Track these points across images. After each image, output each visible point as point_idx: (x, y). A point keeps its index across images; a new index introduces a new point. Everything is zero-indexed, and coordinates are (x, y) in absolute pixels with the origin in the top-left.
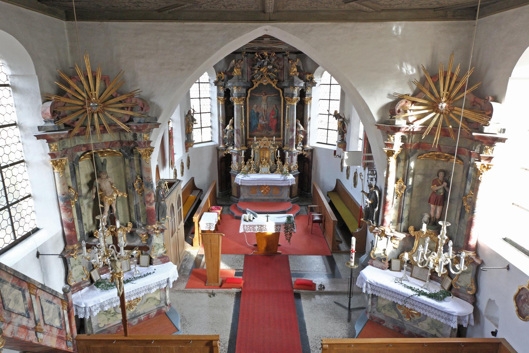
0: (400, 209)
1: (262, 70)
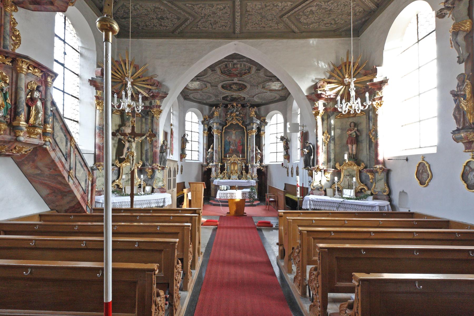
0: (328, 153)
1: (232, 115)
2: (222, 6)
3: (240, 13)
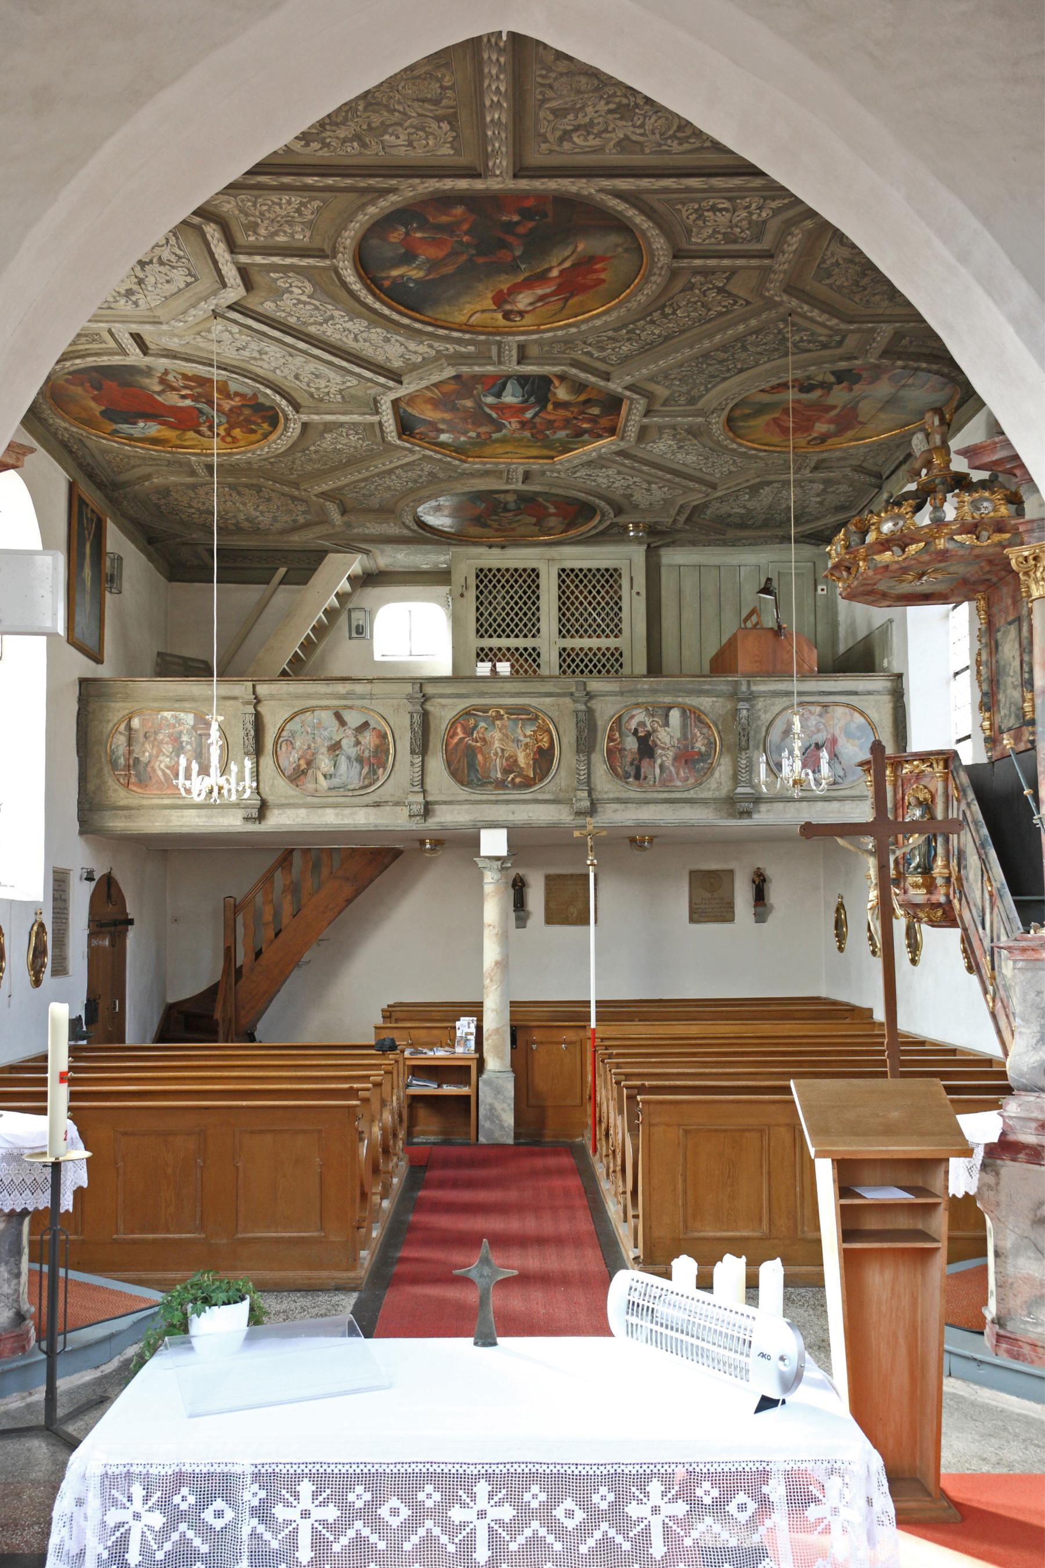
2: (574, 143)
3: (488, 119)
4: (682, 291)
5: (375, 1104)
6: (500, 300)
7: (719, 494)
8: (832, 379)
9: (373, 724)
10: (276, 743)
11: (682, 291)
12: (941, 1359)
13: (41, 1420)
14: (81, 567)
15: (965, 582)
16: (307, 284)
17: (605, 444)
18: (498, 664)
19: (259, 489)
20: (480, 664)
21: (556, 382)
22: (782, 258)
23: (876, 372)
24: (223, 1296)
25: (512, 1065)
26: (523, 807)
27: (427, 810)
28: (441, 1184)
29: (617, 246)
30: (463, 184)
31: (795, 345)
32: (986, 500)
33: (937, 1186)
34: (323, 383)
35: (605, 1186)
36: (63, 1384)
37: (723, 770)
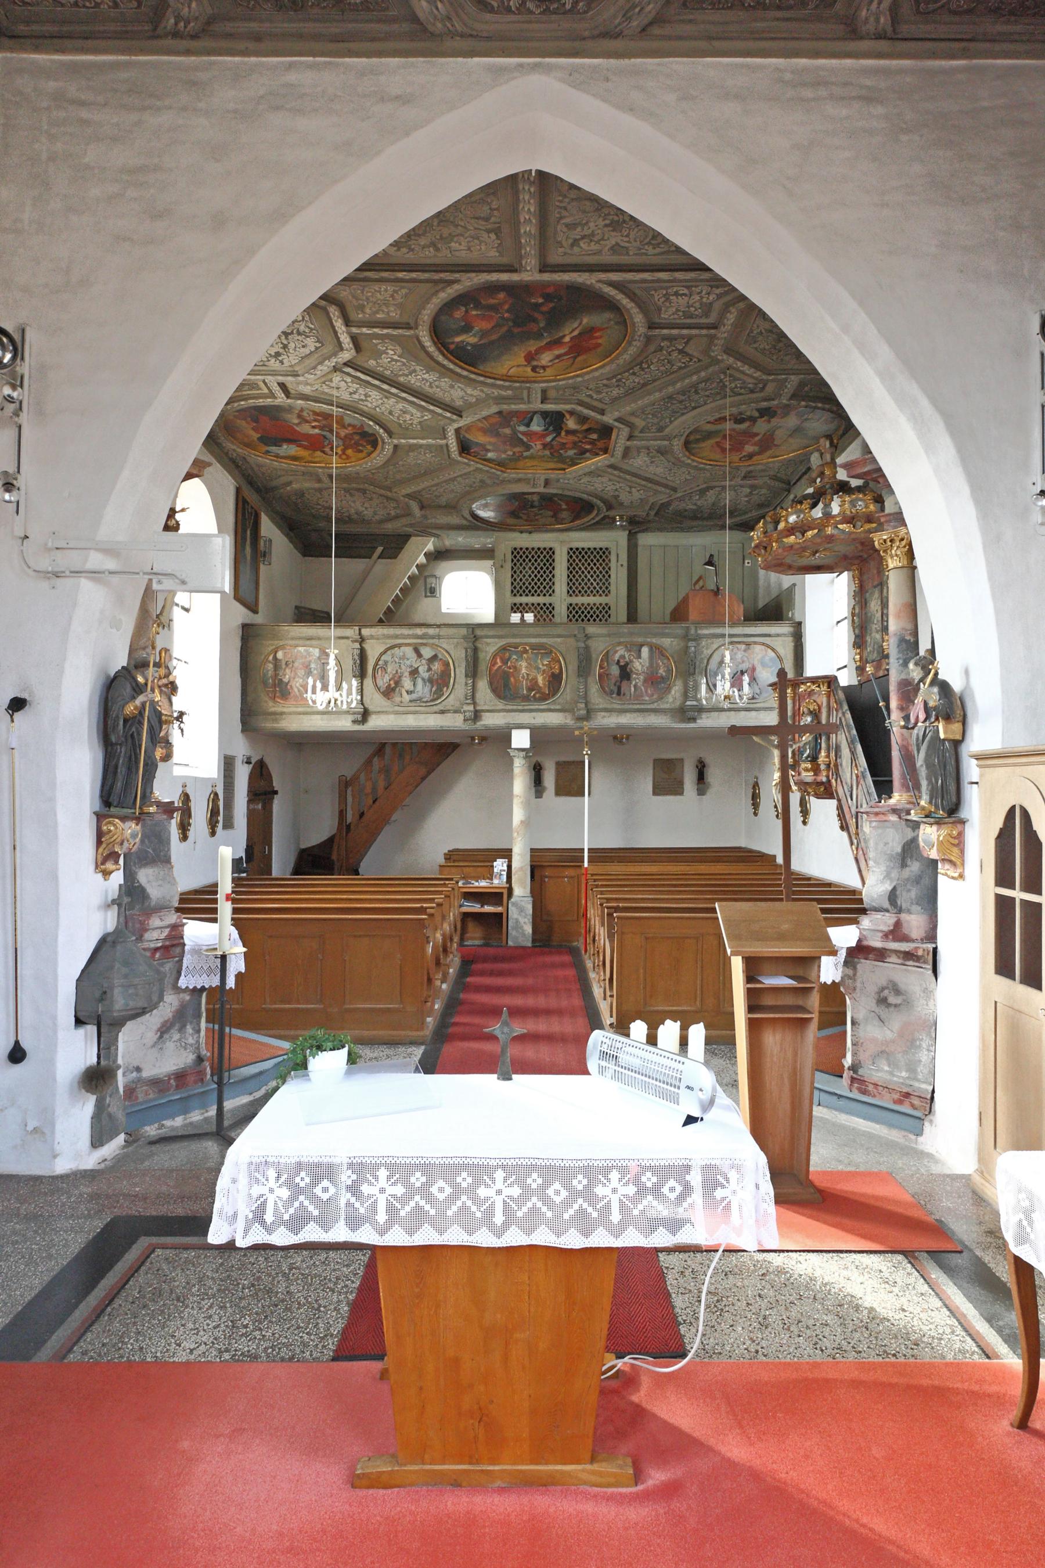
3: (522, 231)
4: (655, 352)
5: (438, 918)
6: (530, 358)
7: (679, 495)
8: (757, 414)
9: (440, 656)
10: (374, 669)
11: (655, 352)
12: (812, 1094)
13: (214, 1128)
14: (244, 548)
15: (845, 557)
16: (398, 347)
17: (600, 460)
18: (526, 615)
19: (364, 491)
20: (513, 615)
21: (568, 416)
22: (723, 329)
23: (787, 409)
24: (330, 1045)
25: (532, 892)
26: (540, 714)
27: (477, 715)
28: (482, 973)
29: (610, 320)
30: (504, 277)
31: (732, 390)
32: (861, 500)
33: (813, 976)
34: (408, 417)
35: (592, 975)
36: (228, 1105)
37: (676, 690)
